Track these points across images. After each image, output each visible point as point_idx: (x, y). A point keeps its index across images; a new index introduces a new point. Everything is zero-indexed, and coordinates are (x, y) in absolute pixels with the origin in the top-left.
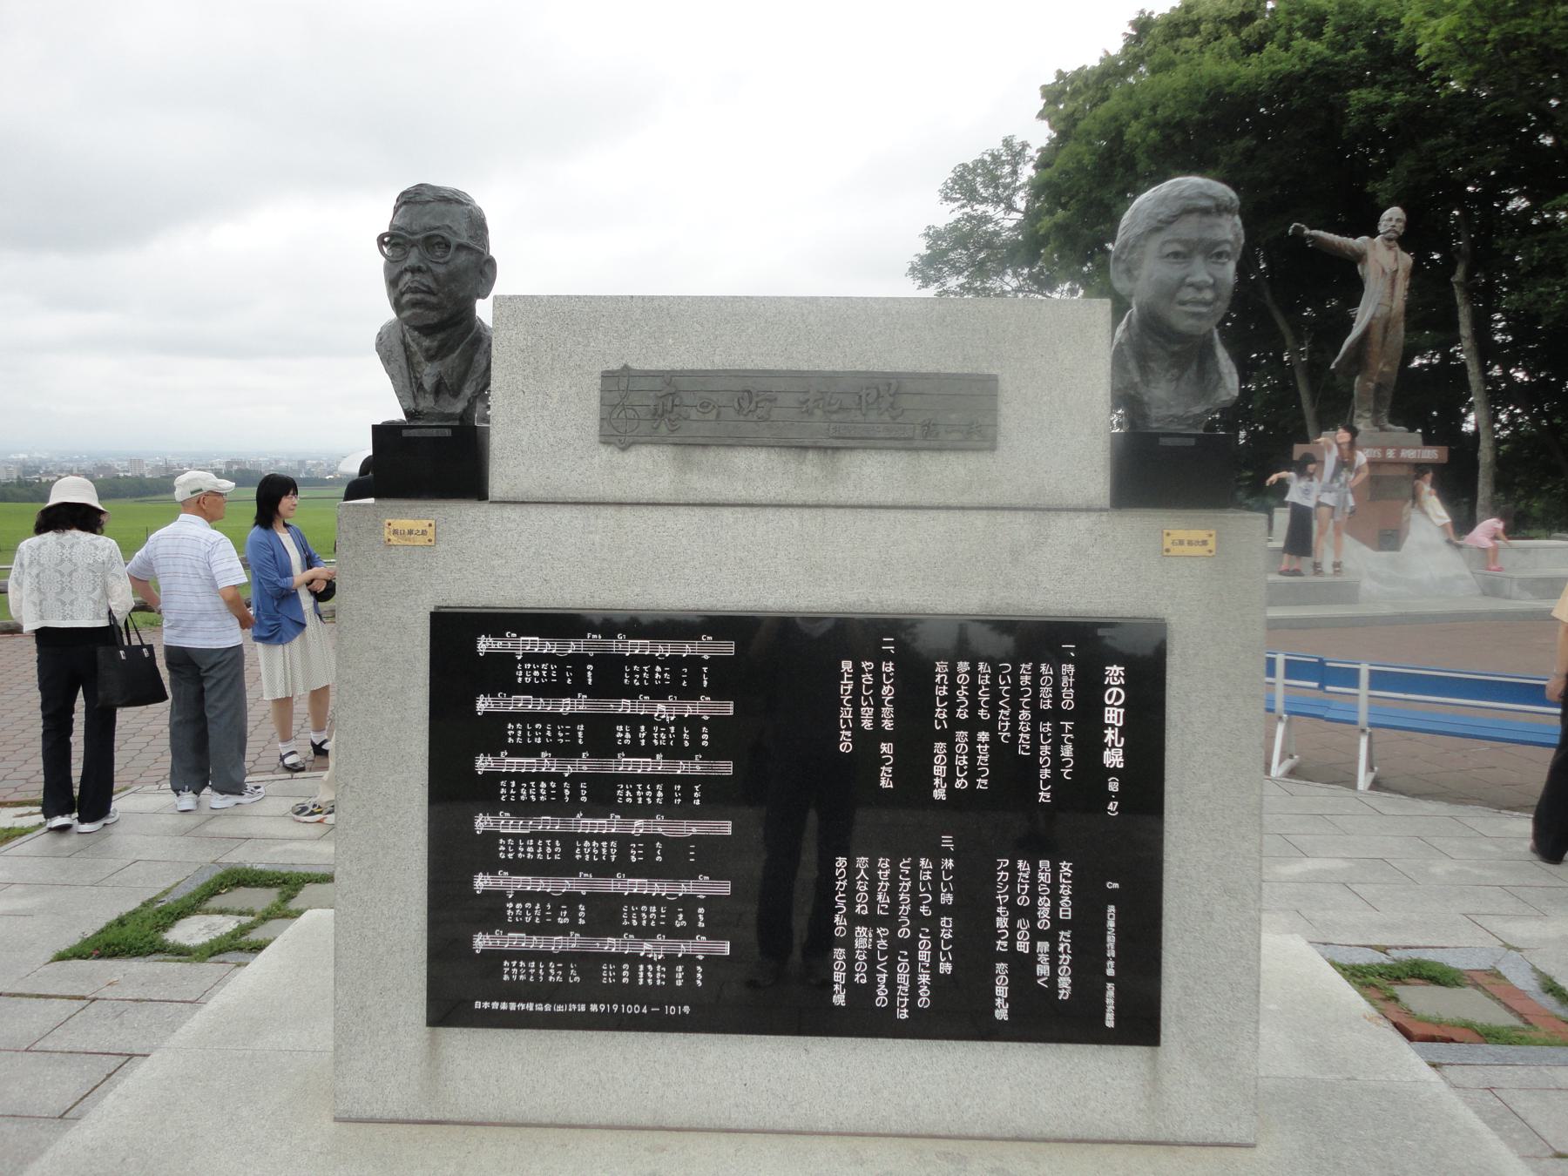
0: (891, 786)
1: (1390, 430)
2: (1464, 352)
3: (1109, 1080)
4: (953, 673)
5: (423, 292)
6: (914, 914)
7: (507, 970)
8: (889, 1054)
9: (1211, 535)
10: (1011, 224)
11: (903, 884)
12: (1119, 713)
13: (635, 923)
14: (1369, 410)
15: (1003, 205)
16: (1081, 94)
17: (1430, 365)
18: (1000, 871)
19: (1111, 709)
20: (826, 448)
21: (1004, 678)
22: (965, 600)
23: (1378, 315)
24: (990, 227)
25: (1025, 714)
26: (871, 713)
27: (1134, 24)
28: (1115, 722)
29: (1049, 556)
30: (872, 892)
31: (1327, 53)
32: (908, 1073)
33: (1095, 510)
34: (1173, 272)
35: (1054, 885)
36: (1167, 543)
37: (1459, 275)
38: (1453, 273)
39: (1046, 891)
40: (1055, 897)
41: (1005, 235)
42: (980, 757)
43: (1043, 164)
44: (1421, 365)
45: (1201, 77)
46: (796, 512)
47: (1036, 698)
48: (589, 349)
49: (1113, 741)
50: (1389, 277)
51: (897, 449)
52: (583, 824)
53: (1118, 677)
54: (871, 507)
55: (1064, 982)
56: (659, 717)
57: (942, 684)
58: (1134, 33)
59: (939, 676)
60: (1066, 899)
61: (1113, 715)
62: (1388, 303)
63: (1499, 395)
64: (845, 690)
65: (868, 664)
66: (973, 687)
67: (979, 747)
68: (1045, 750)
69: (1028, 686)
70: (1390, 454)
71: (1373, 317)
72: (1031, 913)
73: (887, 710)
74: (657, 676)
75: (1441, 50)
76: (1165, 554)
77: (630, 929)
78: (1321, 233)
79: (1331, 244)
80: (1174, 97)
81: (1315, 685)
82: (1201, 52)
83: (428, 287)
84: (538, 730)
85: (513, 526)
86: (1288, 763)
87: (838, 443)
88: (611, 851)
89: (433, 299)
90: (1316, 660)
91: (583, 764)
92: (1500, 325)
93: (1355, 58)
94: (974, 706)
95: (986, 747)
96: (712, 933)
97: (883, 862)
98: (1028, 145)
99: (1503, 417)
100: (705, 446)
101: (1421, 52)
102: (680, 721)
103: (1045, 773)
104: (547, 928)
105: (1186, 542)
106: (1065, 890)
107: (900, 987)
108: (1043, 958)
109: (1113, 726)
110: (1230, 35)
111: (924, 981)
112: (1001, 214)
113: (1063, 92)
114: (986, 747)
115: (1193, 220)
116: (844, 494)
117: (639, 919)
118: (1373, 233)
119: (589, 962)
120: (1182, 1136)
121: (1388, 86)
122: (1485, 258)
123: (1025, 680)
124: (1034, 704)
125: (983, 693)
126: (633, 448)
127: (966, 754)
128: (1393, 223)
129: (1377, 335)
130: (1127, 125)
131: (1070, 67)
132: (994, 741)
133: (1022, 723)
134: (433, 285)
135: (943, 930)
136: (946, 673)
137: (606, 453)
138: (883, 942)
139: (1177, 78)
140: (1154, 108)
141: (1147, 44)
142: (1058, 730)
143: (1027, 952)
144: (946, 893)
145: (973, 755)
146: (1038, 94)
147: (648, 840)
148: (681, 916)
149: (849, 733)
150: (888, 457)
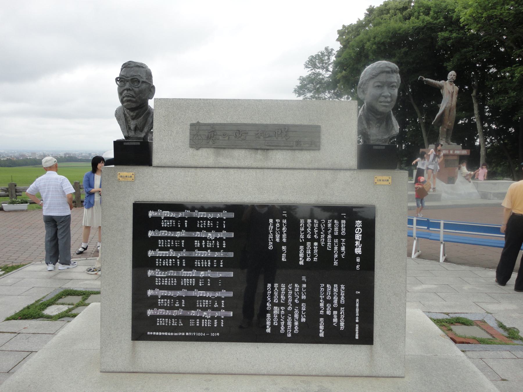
0: (286, 260)
1: (451, 144)
2: (475, 119)
4: (306, 223)
5: (131, 97)
6: (293, 302)
8: (285, 348)
9: (390, 178)
10: (328, 76)
11: (290, 292)
12: (360, 236)
13: (201, 306)
14: (444, 138)
15: (325, 70)
16: (351, 33)
17: (465, 123)
18: (321, 288)
19: (357, 235)
20: (264, 149)
21: (323, 225)
23: (447, 106)
24: (321, 77)
25: (329, 237)
26: (279, 236)
27: (368, 10)
28: (359, 239)
30: (279, 295)
31: (431, 20)
33: (352, 170)
34: (378, 92)
35: (339, 293)
37: (474, 93)
38: (472, 93)
39: (336, 294)
40: (339, 296)
41: (326, 79)
42: (315, 251)
43: (338, 56)
44: (462, 123)
45: (390, 28)
46: (254, 170)
49: (358, 245)
50: (451, 94)
51: (288, 150)
52: (184, 273)
54: (279, 169)
55: (342, 324)
56: (209, 238)
57: (302, 227)
58: (368, 13)
59: (301, 224)
60: (343, 297)
61: (358, 237)
62: (451, 103)
63: (487, 133)
64: (271, 229)
65: (278, 220)
66: (312, 228)
67: (314, 247)
68: (336, 248)
69: (330, 227)
70: (451, 152)
71: (446, 107)
72: (331, 302)
73: (284, 235)
74: (208, 224)
75: (468, 20)
76: (375, 184)
77: (199, 308)
78: (429, 80)
79: (432, 83)
80: (381, 34)
81: (426, 228)
82: (390, 19)
83: (132, 95)
86: (417, 254)
88: (193, 282)
89: (134, 99)
90: (426, 220)
91: (184, 253)
92: (487, 110)
93: (440, 22)
94: (313, 234)
95: (317, 247)
97: (283, 285)
98: (333, 50)
99: (488, 140)
101: (462, 20)
102: (216, 239)
103: (336, 256)
106: (342, 294)
108: (335, 316)
109: (358, 240)
110: (399, 14)
112: (324, 73)
113: (345, 32)
114: (317, 247)
115: (384, 75)
116: (270, 164)
117: (202, 305)
118: (446, 79)
119: (186, 319)
120: (380, 374)
121: (451, 31)
122: (482, 88)
123: (329, 225)
125: (316, 230)
126: (201, 149)
128: (452, 76)
129: (447, 112)
130: (366, 43)
131: (347, 24)
134: (134, 95)
139: (382, 28)
140: (374, 38)
141: (372, 17)
142: (340, 242)
144: (304, 295)
145: (312, 250)
146: (337, 33)
147: (205, 278)
149: (272, 243)
150: (285, 152)
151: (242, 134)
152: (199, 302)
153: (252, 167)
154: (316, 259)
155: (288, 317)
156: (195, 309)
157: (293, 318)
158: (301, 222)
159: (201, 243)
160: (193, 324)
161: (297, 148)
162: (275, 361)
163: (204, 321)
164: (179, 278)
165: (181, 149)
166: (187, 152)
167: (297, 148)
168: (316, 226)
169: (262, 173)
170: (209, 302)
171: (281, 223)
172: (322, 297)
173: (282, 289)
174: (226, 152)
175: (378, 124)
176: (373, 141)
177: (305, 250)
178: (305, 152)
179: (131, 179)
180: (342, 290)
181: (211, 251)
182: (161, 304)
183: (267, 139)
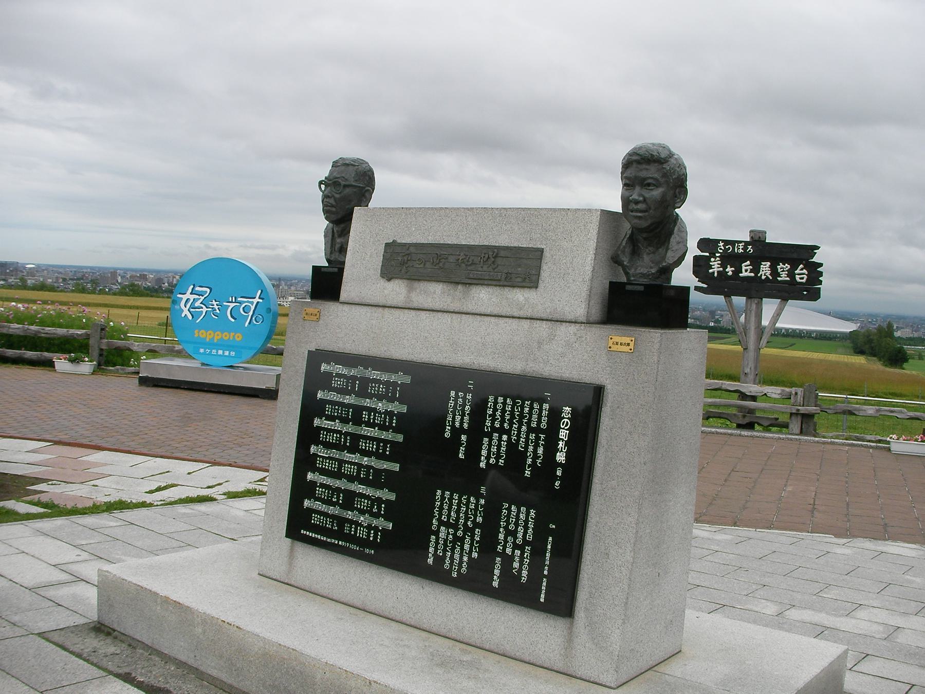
0: (463, 458)
3: (548, 635)
4: (496, 403)
5: (330, 206)
6: (465, 524)
7: (313, 518)
8: (455, 598)
11: (462, 508)
12: (566, 433)
13: (359, 507)
18: (504, 509)
19: (563, 430)
20: (466, 284)
21: (517, 408)
22: (515, 367)
25: (524, 428)
26: (459, 419)
28: (564, 438)
29: (555, 346)
30: (450, 510)
32: (462, 610)
33: (579, 323)
35: (526, 521)
36: (611, 342)
39: (522, 524)
40: (526, 528)
42: (502, 448)
46: (450, 315)
47: (530, 420)
48: (384, 232)
49: (562, 448)
51: (496, 286)
52: (347, 456)
53: (568, 414)
54: (481, 315)
55: (525, 573)
56: (379, 409)
57: (490, 408)
59: (490, 403)
60: (531, 530)
61: (563, 434)
64: (451, 406)
65: (461, 394)
66: (504, 411)
67: (502, 443)
68: (531, 448)
69: (527, 413)
72: (514, 534)
73: (466, 418)
74: (381, 389)
76: (609, 349)
77: (357, 509)
83: (331, 204)
84: (336, 409)
85: (345, 314)
87: (469, 281)
88: (353, 470)
89: (334, 209)
91: (350, 428)
94: (503, 421)
95: (505, 443)
96: (387, 518)
97: (456, 496)
100: (419, 280)
102: (387, 413)
103: (529, 461)
104: (328, 502)
105: (619, 344)
106: (531, 526)
107: (455, 561)
108: (517, 559)
109: (563, 440)
111: (465, 560)
114: (505, 443)
116: (470, 307)
117: (361, 505)
119: (342, 521)
120: (579, 674)
123: (526, 410)
124: (529, 423)
125: (507, 415)
126: (392, 280)
127: (496, 446)
132: (509, 439)
133: (522, 433)
134: (334, 203)
135: (476, 536)
136: (493, 402)
137: (383, 283)
138: (451, 536)
142: (538, 438)
143: (510, 554)
144: (480, 516)
145: (499, 446)
147: (369, 467)
148: (376, 507)
149: (449, 428)
150: (490, 290)
151: (440, 259)
152: (358, 501)
153: (448, 310)
154: (503, 461)
155: (456, 546)
156: (352, 509)
157: (462, 549)
158: (490, 400)
159: (369, 415)
160: (348, 530)
161: (506, 283)
162: (441, 614)
163: (360, 530)
164: (341, 462)
165: (372, 280)
166: (378, 284)
167: (506, 283)
168: (508, 408)
169: (459, 319)
170: (368, 503)
171: (464, 398)
172: (503, 524)
173: (454, 501)
174: (423, 285)
175: (650, 248)
176: (633, 276)
177: (490, 445)
178: (517, 290)
179: (316, 317)
180: (531, 518)
181: (378, 429)
182: (318, 494)
183: (469, 268)
